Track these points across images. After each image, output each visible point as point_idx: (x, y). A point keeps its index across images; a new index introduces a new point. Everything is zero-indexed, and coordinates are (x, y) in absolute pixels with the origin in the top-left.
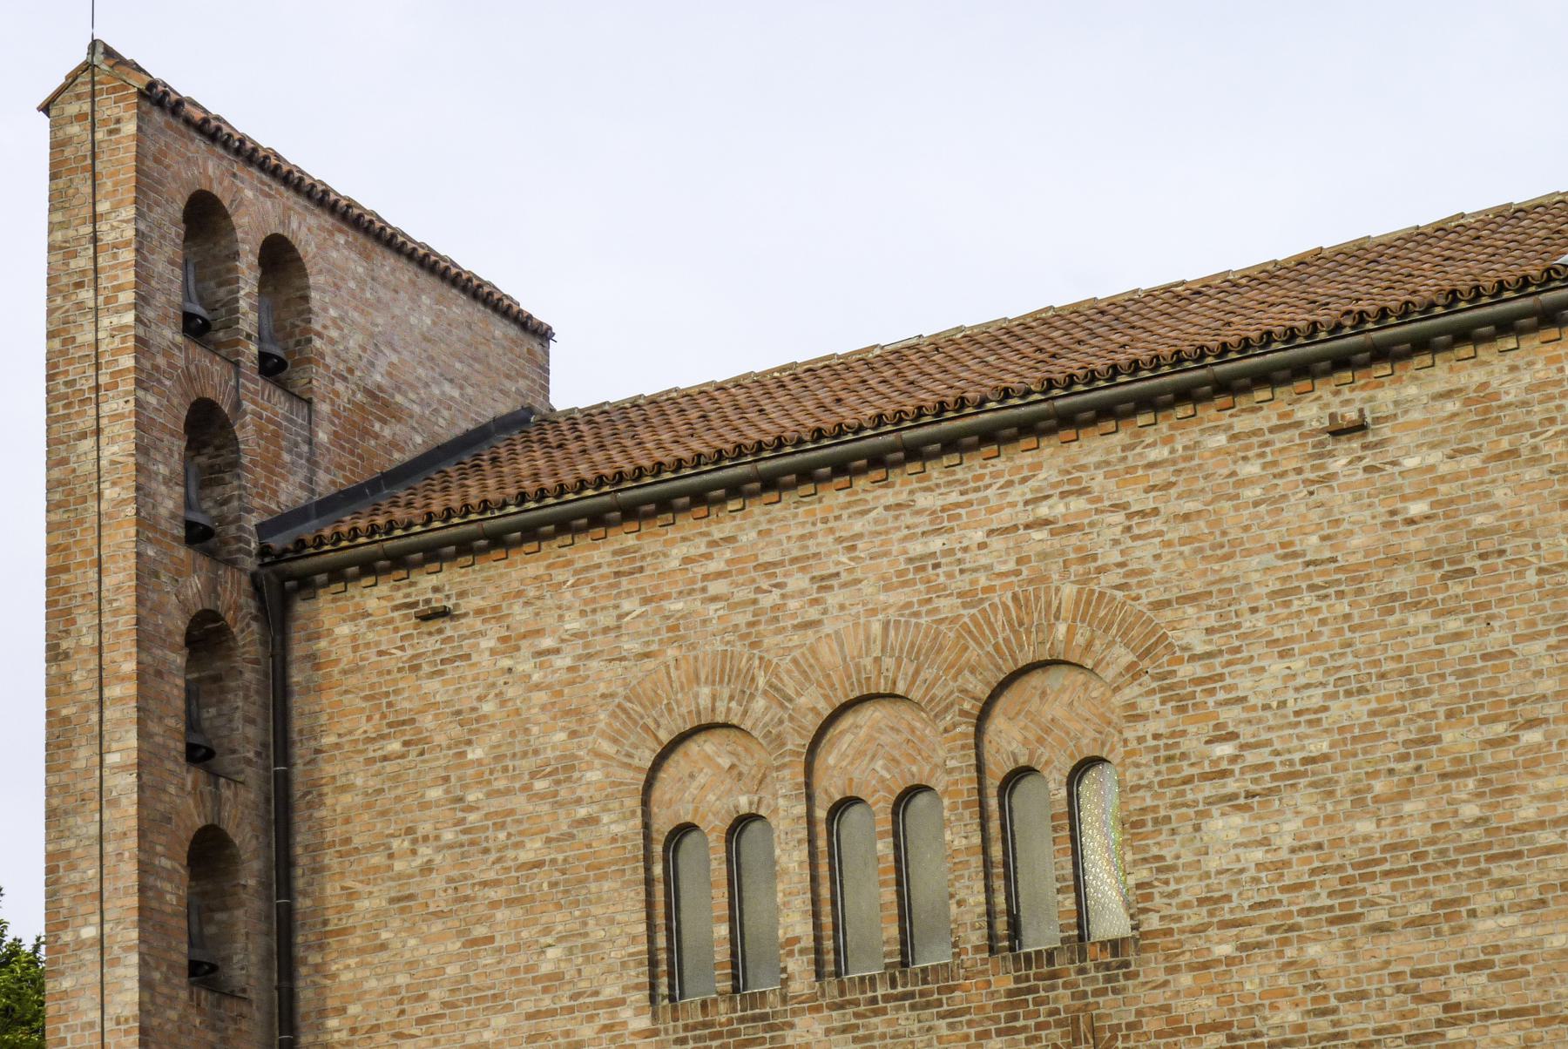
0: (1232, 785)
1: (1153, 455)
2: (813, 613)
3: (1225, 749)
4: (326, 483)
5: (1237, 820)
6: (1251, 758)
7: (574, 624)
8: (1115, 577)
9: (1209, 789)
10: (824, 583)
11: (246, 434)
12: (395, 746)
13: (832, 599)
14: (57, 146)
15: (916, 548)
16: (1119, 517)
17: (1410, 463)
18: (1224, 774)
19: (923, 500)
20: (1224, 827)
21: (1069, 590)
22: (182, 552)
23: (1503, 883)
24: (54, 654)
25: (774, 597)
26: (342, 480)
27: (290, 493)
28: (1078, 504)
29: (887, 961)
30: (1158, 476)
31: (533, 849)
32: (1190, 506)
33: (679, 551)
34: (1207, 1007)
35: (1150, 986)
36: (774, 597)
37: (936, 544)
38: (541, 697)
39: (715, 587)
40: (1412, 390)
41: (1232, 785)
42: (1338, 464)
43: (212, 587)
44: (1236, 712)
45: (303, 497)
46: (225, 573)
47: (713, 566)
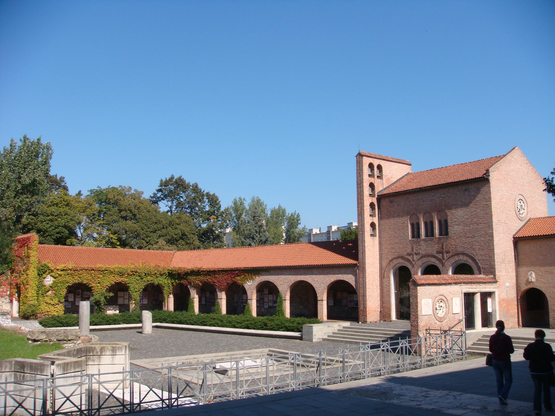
0: (456, 223)
1: (451, 191)
2: (422, 204)
3: (456, 219)
4: (385, 187)
5: (457, 226)
6: (458, 220)
7: (403, 204)
8: (448, 202)
9: (455, 223)
10: (423, 201)
11: (375, 185)
12: (389, 214)
13: (424, 203)
14: (357, 160)
15: (431, 199)
16: (448, 197)
17: (472, 193)
18: (456, 222)
19: (432, 194)
20: (456, 227)
21: (444, 204)
22: (369, 197)
23: (478, 234)
24: (358, 208)
25: (419, 202)
26: (387, 186)
27: (381, 189)
28: (444, 195)
29: (437, 231)
30: (451, 193)
31: (400, 224)
32: (453, 196)
33: (412, 197)
34: (454, 243)
35: (277, 356)
36: (419, 202)
37: (433, 198)
38: (400, 210)
39: (415, 201)
40: (472, 186)
41: (456, 223)
42: (466, 193)
43: (372, 200)
44: (457, 216)
45: (382, 189)
46: (374, 198)
47: (415, 199)
